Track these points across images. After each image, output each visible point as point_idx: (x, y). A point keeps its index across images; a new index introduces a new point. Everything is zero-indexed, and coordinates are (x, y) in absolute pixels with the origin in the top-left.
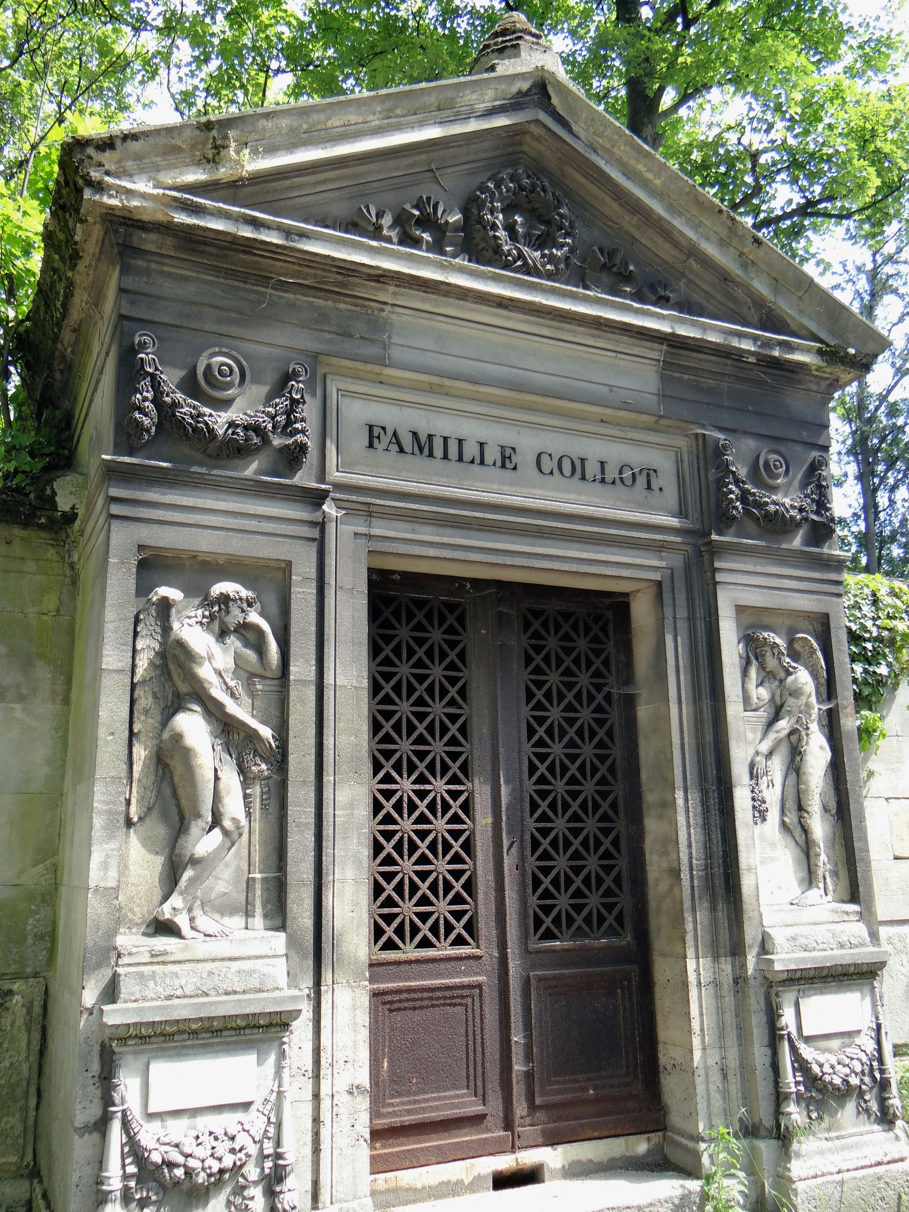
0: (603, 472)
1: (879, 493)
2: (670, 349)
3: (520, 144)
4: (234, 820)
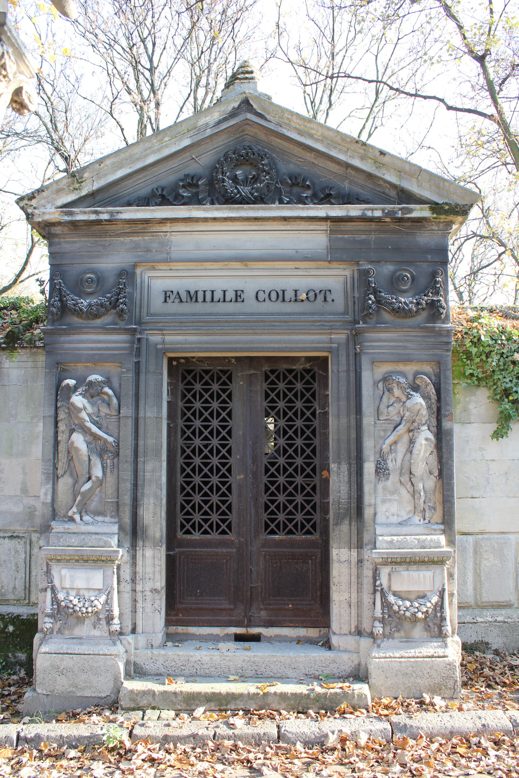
0: (296, 296)
2: (333, 224)
3: (243, 131)
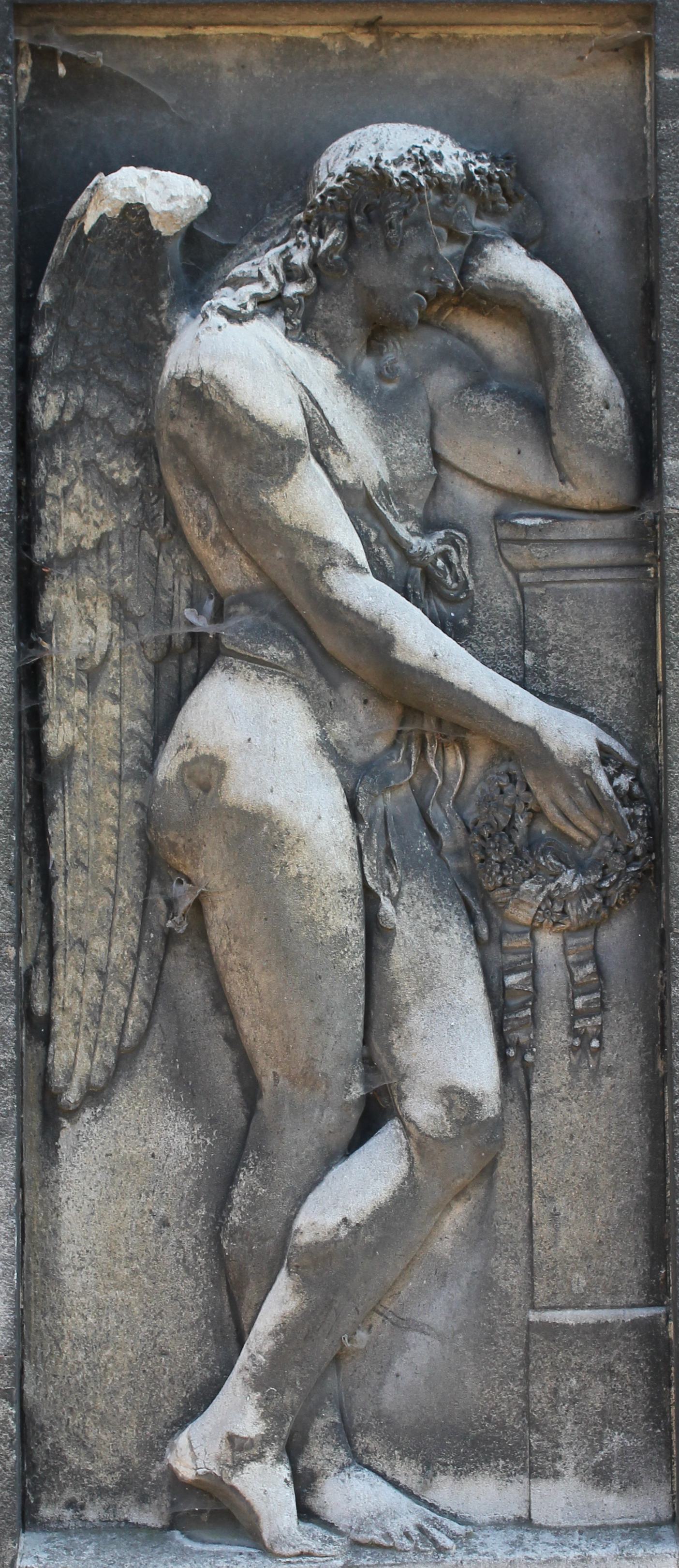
1: (244, 503)
4: (452, 1095)
